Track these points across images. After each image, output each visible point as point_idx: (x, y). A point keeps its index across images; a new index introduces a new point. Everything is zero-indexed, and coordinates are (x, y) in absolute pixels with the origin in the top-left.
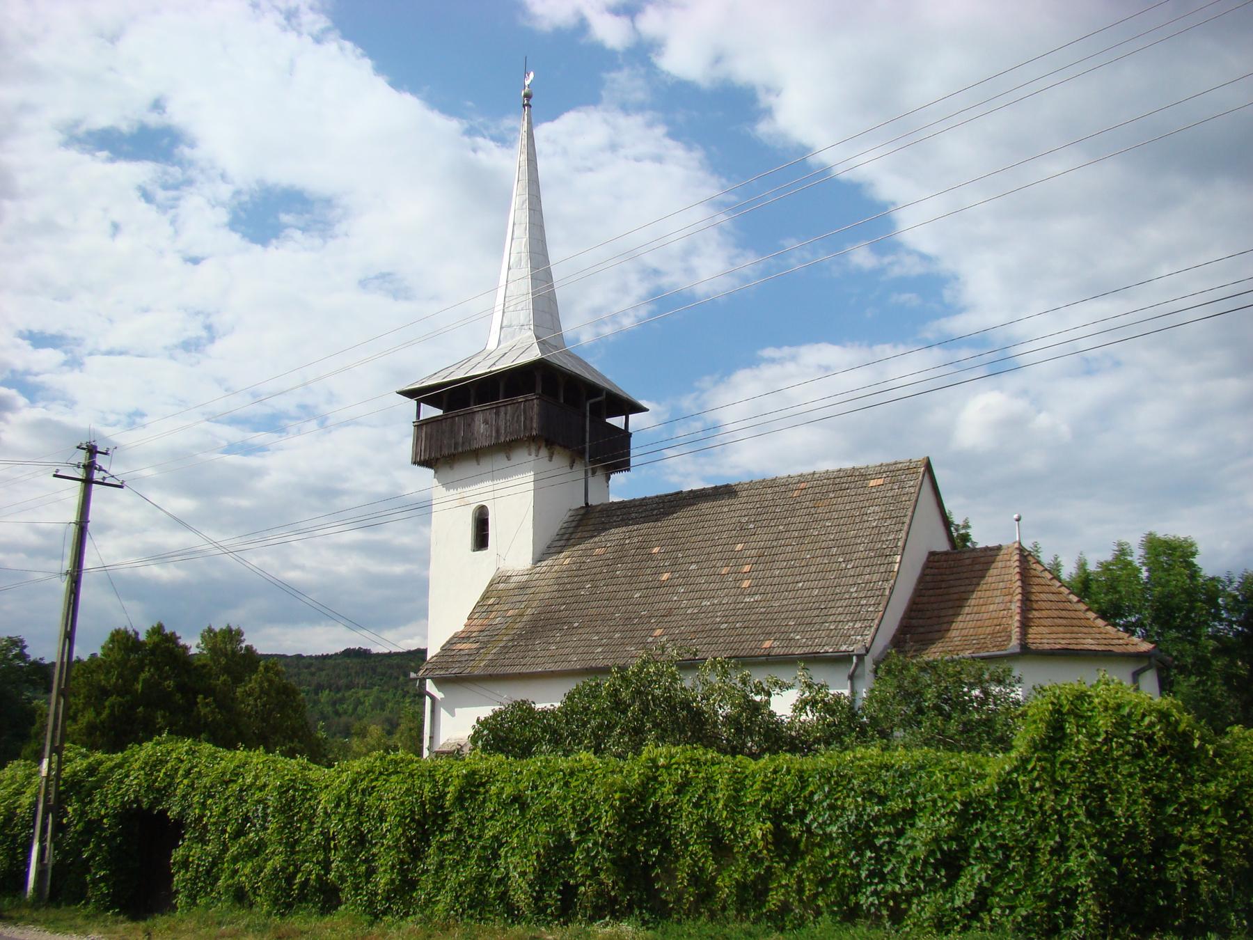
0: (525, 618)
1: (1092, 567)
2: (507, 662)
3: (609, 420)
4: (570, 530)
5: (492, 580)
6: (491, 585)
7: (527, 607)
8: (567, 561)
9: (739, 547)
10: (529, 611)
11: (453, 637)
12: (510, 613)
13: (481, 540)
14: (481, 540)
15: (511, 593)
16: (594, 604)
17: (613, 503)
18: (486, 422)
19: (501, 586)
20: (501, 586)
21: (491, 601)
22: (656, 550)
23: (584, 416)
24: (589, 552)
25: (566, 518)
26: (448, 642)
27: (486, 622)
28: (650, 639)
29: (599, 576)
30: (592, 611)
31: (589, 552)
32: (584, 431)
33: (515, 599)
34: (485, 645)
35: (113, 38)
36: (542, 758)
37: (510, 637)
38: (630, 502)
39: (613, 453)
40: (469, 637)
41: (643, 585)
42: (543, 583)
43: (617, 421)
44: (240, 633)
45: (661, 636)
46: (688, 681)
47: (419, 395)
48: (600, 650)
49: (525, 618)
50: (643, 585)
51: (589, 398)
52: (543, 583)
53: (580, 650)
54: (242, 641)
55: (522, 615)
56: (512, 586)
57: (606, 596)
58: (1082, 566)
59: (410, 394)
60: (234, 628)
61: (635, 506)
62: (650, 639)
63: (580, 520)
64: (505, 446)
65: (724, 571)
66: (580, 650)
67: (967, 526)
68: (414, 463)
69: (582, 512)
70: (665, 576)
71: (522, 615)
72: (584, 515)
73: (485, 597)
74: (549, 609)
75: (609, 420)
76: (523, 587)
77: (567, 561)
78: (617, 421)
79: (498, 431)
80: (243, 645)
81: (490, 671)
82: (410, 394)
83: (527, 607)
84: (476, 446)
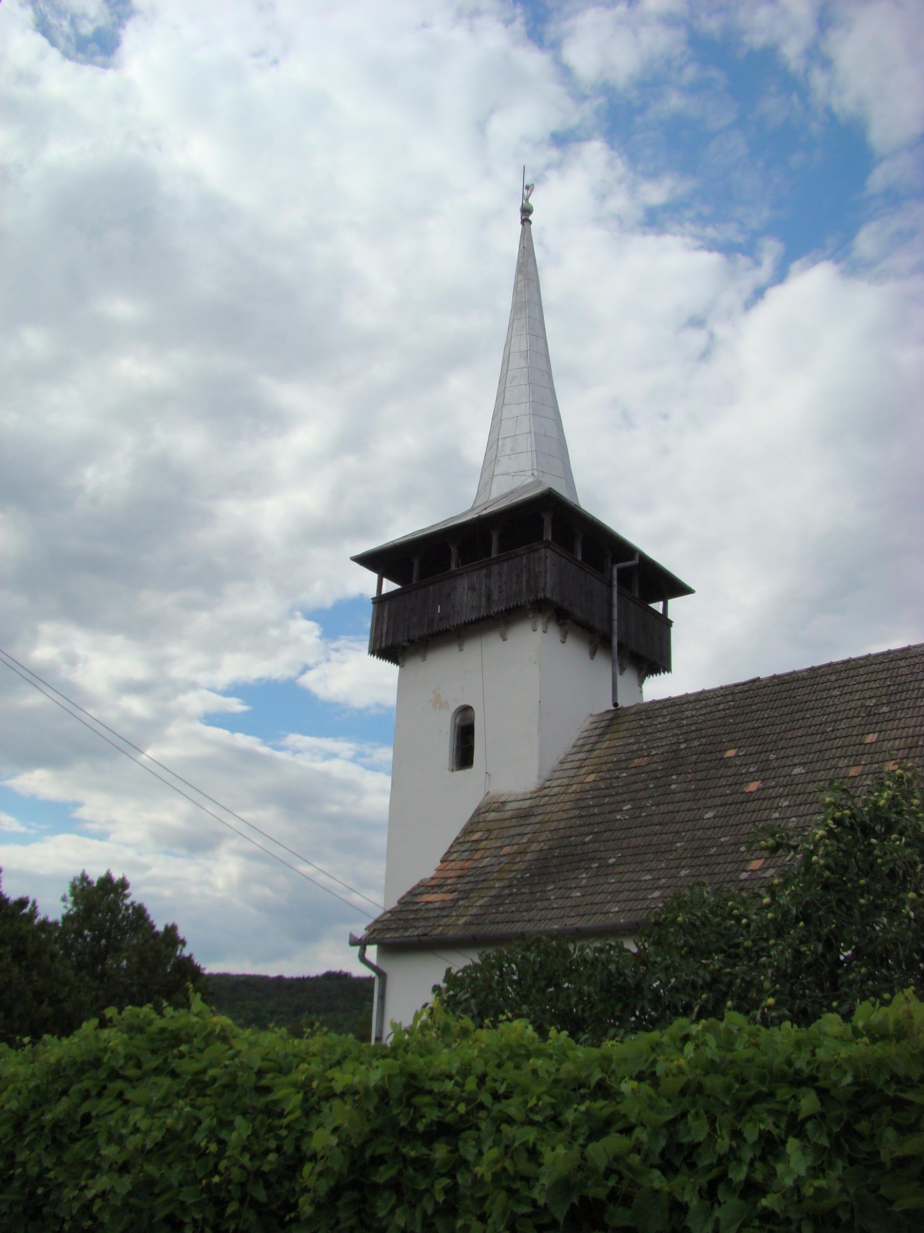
0: (528, 857)
2: (500, 917)
4: (593, 739)
5: (478, 809)
6: (478, 812)
7: (531, 841)
8: (591, 777)
9: (871, 738)
10: (535, 846)
11: (419, 886)
12: (506, 850)
13: (464, 755)
14: (464, 755)
15: (507, 823)
16: (638, 831)
17: (654, 702)
18: (472, 588)
19: (492, 816)
20: (492, 816)
21: (476, 836)
22: (730, 753)
23: (610, 585)
24: (624, 765)
25: (586, 725)
26: (410, 893)
27: (468, 864)
28: (744, 875)
29: (643, 794)
30: (640, 841)
31: (624, 765)
32: (611, 606)
33: (512, 832)
34: (466, 895)
35: (579, 1167)
36: (133, 1142)
37: (505, 883)
38: (681, 697)
39: (648, 651)
40: (441, 886)
41: (718, 801)
42: (555, 808)
44: (124, 884)
45: (764, 869)
46: (568, 1066)
48: (657, 894)
49: (528, 857)
50: (718, 801)
51: (615, 562)
52: (555, 808)
53: (624, 896)
54: (126, 896)
55: (523, 853)
56: (507, 815)
57: (656, 819)
60: (117, 876)
61: (689, 702)
62: (744, 875)
63: (607, 726)
64: (498, 619)
65: (853, 772)
66: (624, 896)
69: (609, 716)
70: (753, 786)
71: (523, 853)
72: (612, 719)
73: (468, 830)
74: (566, 842)
76: (524, 815)
77: (591, 777)
79: (489, 597)
80: (128, 901)
81: (474, 930)
83: (531, 841)
84: (456, 621)
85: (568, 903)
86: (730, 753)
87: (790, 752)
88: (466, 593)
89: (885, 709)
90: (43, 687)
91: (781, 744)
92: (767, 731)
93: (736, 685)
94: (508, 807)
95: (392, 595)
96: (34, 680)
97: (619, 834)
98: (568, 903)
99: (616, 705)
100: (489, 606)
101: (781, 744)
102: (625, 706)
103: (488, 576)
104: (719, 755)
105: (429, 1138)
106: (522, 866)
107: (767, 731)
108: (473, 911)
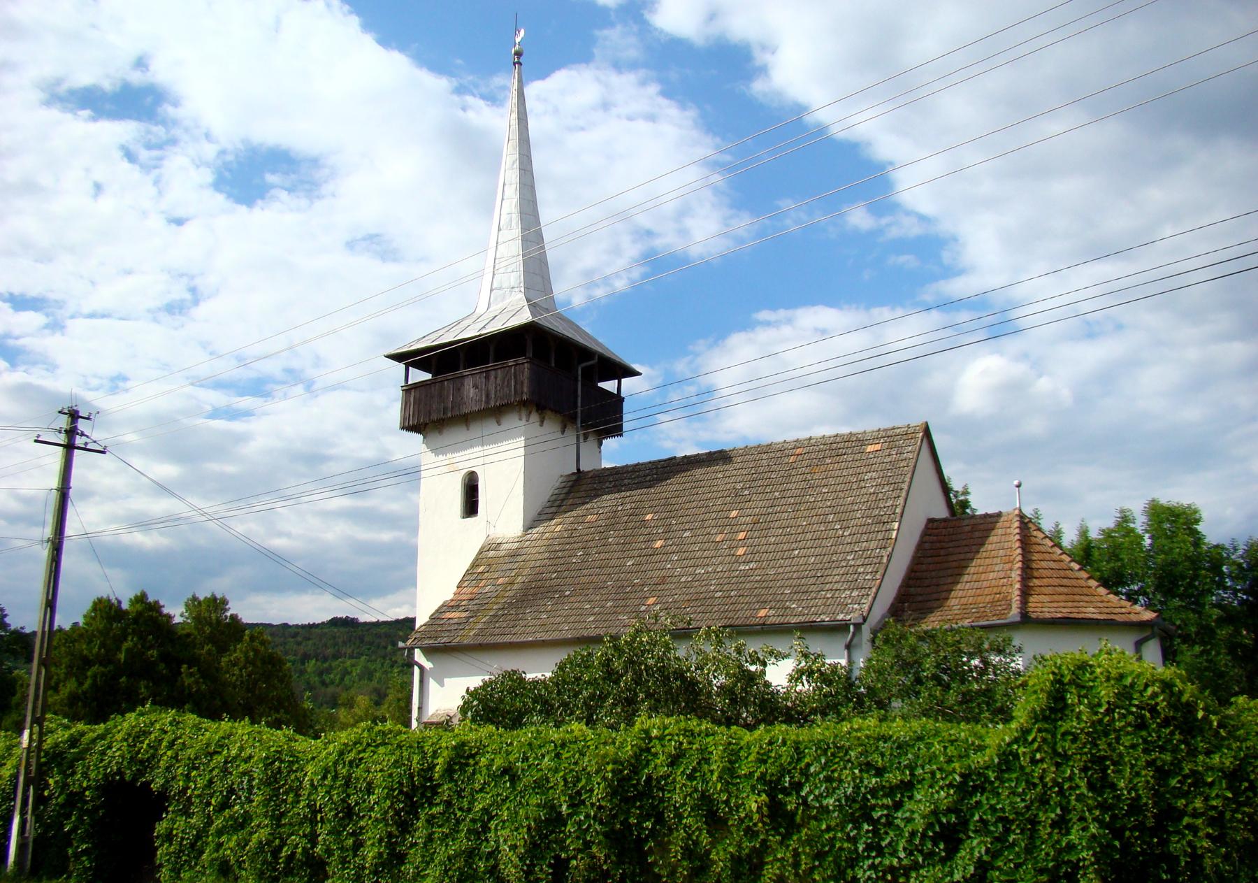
0: (516, 586)
1: (1094, 534)
3: (601, 385)
4: (562, 497)
5: (482, 548)
6: (480, 552)
7: (517, 575)
9: (734, 514)
10: (520, 579)
11: (442, 606)
12: (501, 581)
13: (471, 506)
14: (471, 506)
18: (475, 386)
19: (492, 553)
20: (492, 553)
21: (481, 569)
22: (649, 517)
24: (581, 519)
25: (557, 485)
28: (643, 608)
31: (581, 519)
32: (576, 397)
34: (475, 613)
37: (500, 606)
38: (623, 467)
39: (605, 418)
40: (458, 606)
41: (636, 553)
42: (534, 550)
43: (609, 386)
44: (224, 602)
47: (406, 358)
48: (592, 618)
49: (516, 586)
50: (636, 553)
51: (579, 363)
52: (534, 550)
53: (572, 619)
55: (512, 583)
56: (503, 553)
57: (598, 564)
58: (1084, 533)
59: (398, 357)
60: (219, 596)
61: (627, 472)
62: (643, 608)
63: (572, 487)
64: (495, 411)
66: (572, 619)
67: (966, 493)
68: (403, 428)
69: (574, 478)
70: (659, 544)
71: (512, 583)
72: (575, 481)
73: (475, 565)
75: (601, 385)
76: (513, 554)
78: (609, 386)
79: (488, 396)
81: (480, 640)
82: (398, 357)
83: (517, 575)
84: (465, 410)
85: (539, 622)
86: (649, 517)
87: (685, 519)
88: (472, 388)
89: (747, 492)
90: (302, 573)
91: (680, 513)
92: (673, 501)
93: (660, 461)
94: (504, 547)
95: (417, 386)
96: (309, 577)
97: (573, 573)
98: (539, 622)
99: (578, 470)
100: (487, 402)
101: (680, 513)
102: (586, 469)
103: (487, 378)
104: (641, 518)
105: (468, 758)
106: (510, 594)
107: (673, 501)
108: (480, 626)
